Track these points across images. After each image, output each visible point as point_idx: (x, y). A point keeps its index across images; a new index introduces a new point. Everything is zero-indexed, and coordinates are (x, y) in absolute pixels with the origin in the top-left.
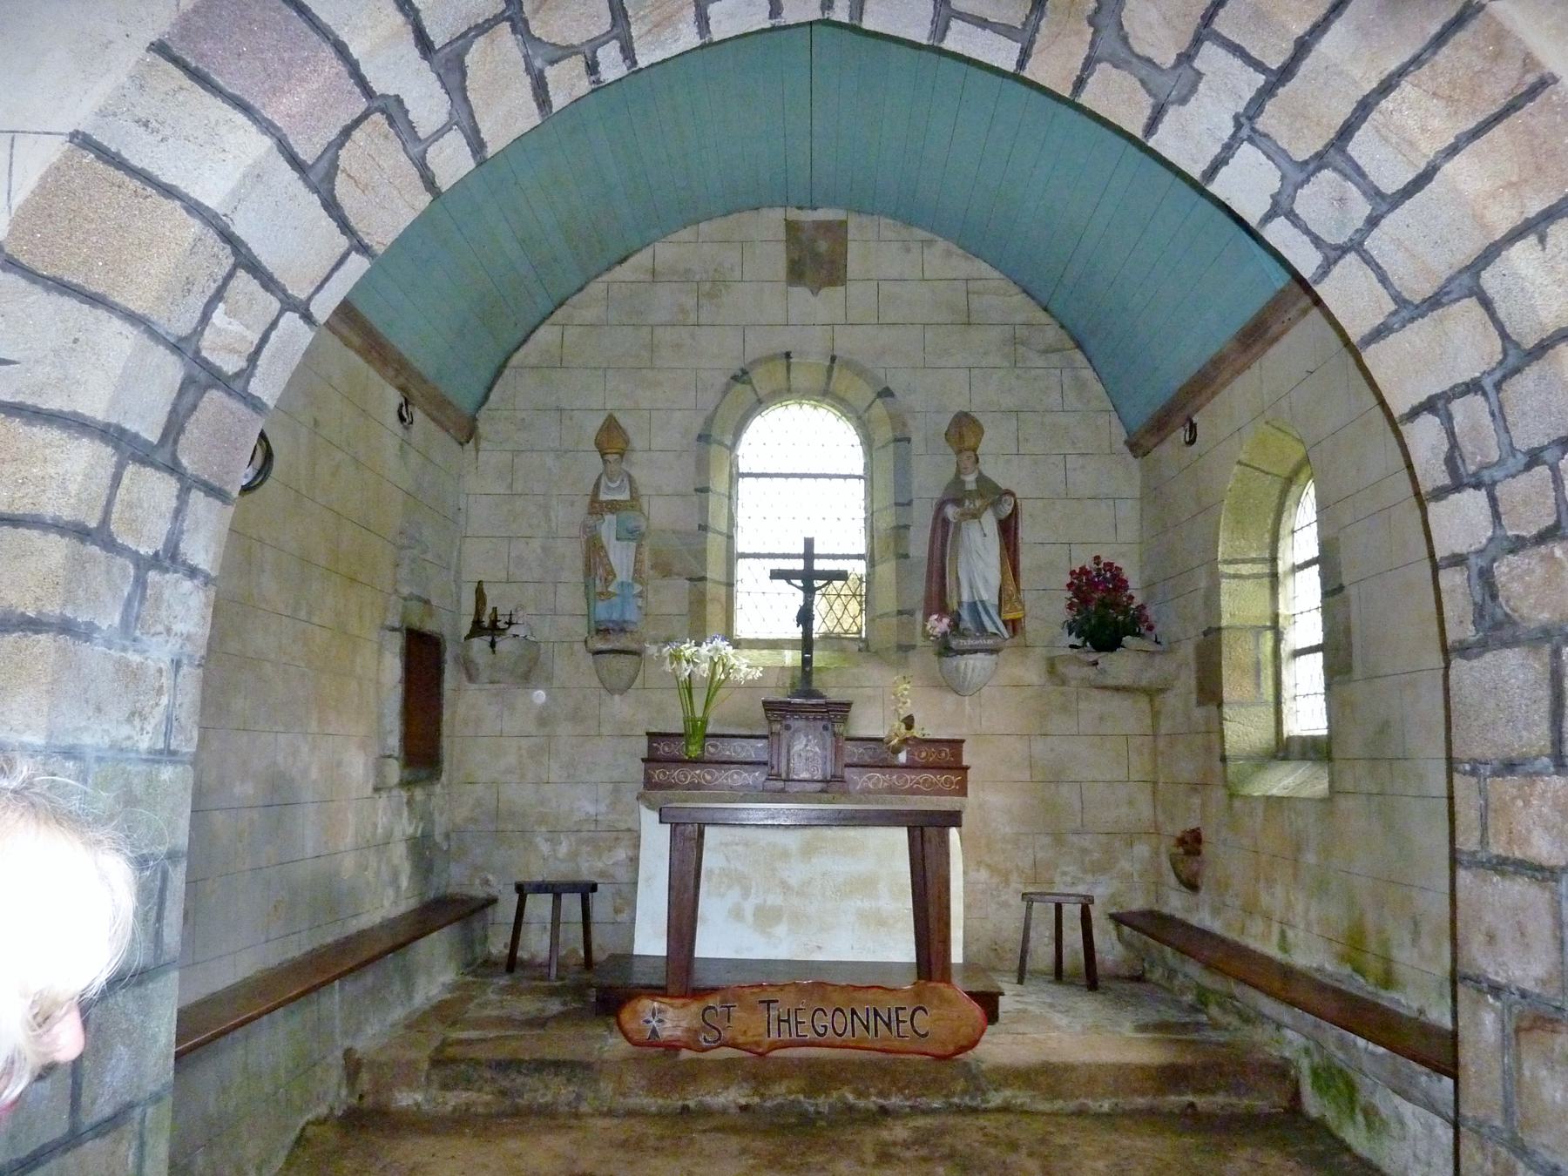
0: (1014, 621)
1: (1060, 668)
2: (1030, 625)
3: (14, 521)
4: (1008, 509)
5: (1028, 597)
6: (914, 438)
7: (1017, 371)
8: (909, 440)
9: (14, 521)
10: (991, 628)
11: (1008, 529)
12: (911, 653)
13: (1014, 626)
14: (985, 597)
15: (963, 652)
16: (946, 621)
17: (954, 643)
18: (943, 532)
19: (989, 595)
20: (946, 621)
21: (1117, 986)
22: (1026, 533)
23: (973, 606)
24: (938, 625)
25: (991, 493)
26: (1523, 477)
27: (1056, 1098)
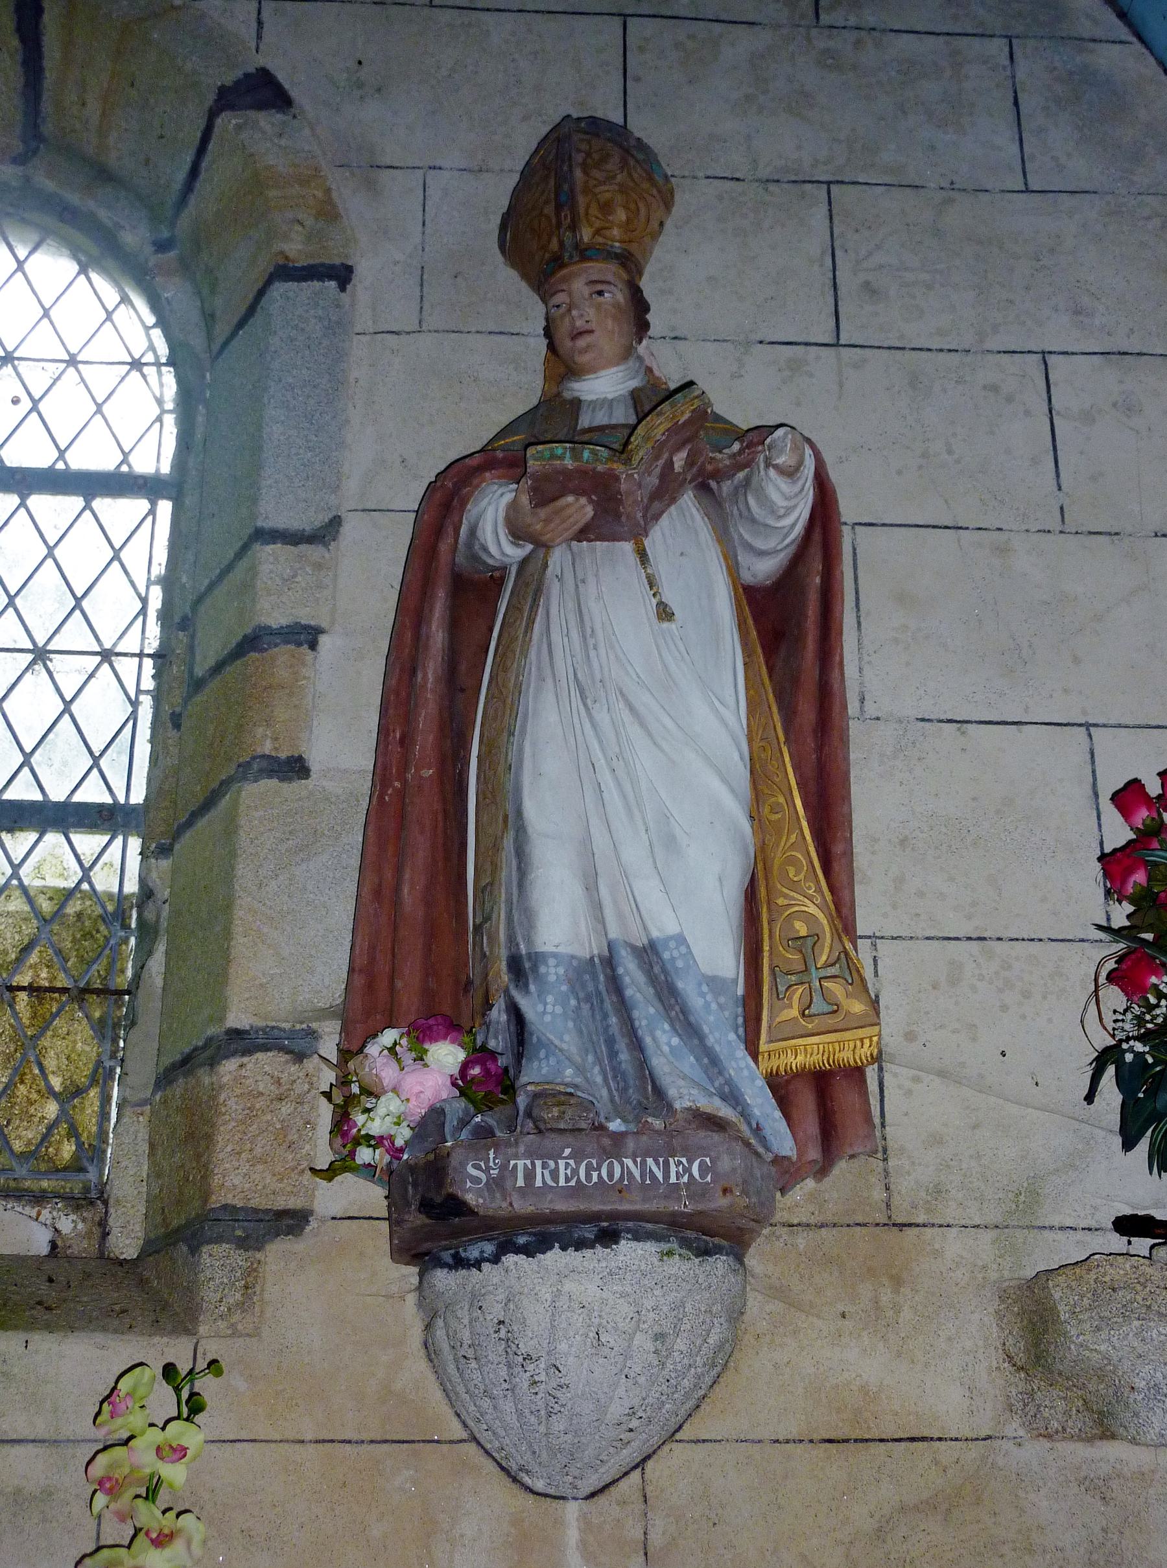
0: (822, 1080)
1: (1087, 1340)
2: (910, 1108)
3: (3, 1441)
4: (785, 505)
5: (894, 972)
6: (365, 269)
7: (821, 42)
8: (343, 275)
9: (3, 1441)
10: (686, 1091)
11: (791, 627)
12: (277, 1252)
13: (830, 1104)
14: (664, 922)
15: (539, 1233)
16: (447, 1055)
17: (473, 1180)
18: (460, 629)
19: (696, 918)
20: (447, 1055)
21: (487, 906)
22: (881, 666)
23: (601, 979)
24: (419, 1080)
25: (711, 456)
26: (1079, 1446)
27: (601, 475)
